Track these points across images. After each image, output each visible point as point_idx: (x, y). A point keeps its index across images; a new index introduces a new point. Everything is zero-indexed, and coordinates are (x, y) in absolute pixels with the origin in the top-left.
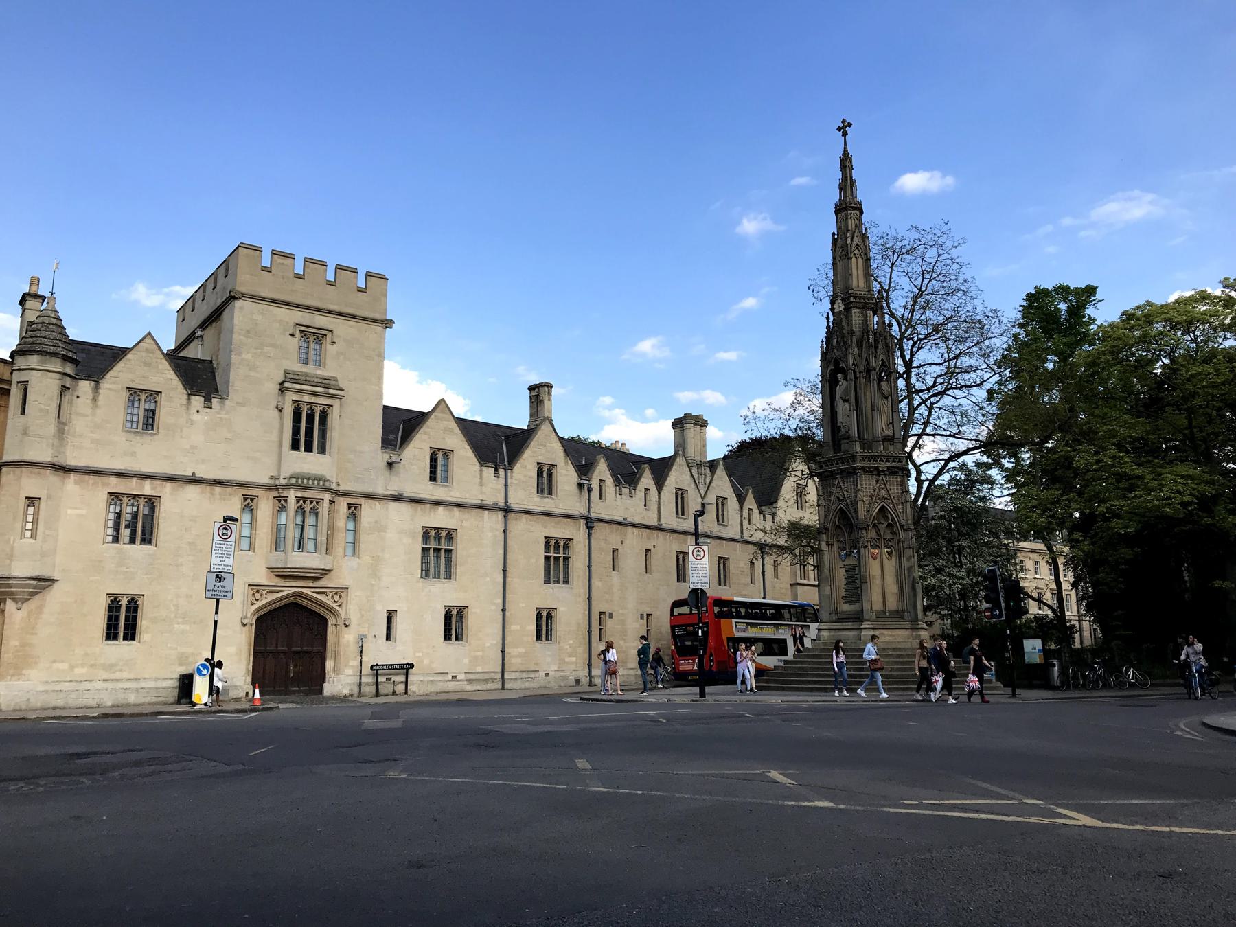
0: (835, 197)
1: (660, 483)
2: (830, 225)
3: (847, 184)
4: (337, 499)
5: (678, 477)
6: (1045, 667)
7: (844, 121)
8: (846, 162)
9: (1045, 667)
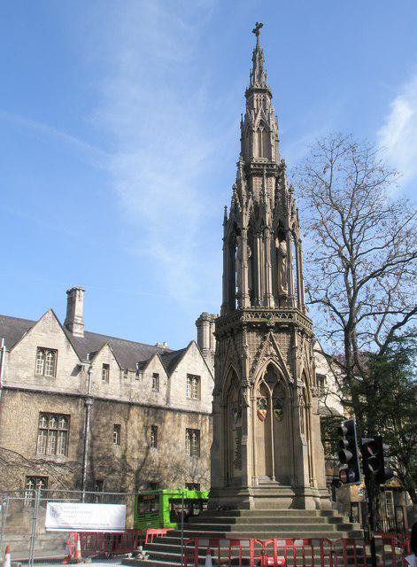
8: (257, 56)
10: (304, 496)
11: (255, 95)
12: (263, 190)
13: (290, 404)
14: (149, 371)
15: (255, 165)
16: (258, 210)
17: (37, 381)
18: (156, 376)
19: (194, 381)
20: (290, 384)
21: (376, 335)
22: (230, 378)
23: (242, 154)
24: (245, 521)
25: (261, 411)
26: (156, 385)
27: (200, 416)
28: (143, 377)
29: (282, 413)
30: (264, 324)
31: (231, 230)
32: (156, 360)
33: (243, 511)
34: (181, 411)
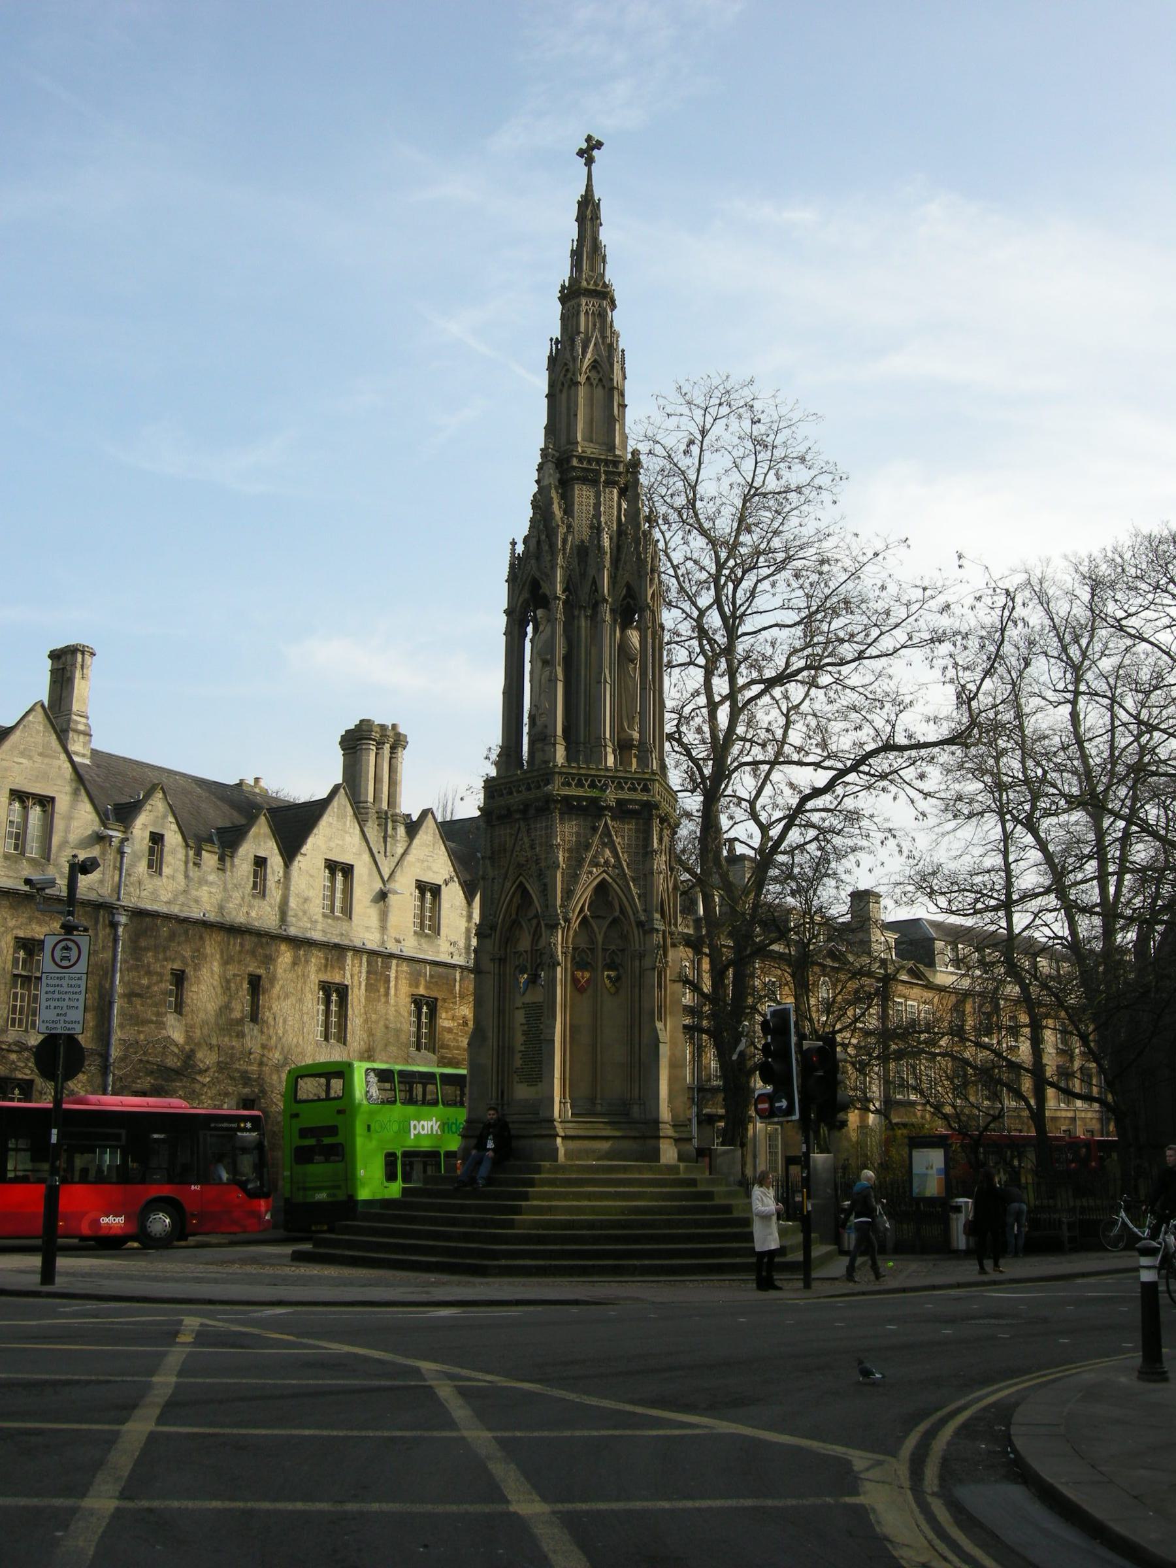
0: (562, 272)
1: (290, 848)
2: (548, 321)
3: (588, 250)
4: (731, 823)
5: (335, 837)
6: (941, 1209)
7: (589, 139)
8: (588, 211)
9: (941, 1209)
10: (658, 1137)
11: (584, 302)
12: (597, 515)
13: (637, 963)
14: (247, 850)
15: (581, 459)
16: (585, 553)
17: (9, 867)
18: (260, 862)
19: (339, 877)
20: (640, 924)
21: (752, 803)
22: (514, 905)
23: (551, 430)
24: (551, 1183)
25: (579, 974)
26: (259, 888)
27: (350, 954)
28: (233, 865)
29: (618, 978)
30: (594, 801)
31: (526, 595)
32: (261, 827)
33: (547, 1164)
34: (309, 943)
